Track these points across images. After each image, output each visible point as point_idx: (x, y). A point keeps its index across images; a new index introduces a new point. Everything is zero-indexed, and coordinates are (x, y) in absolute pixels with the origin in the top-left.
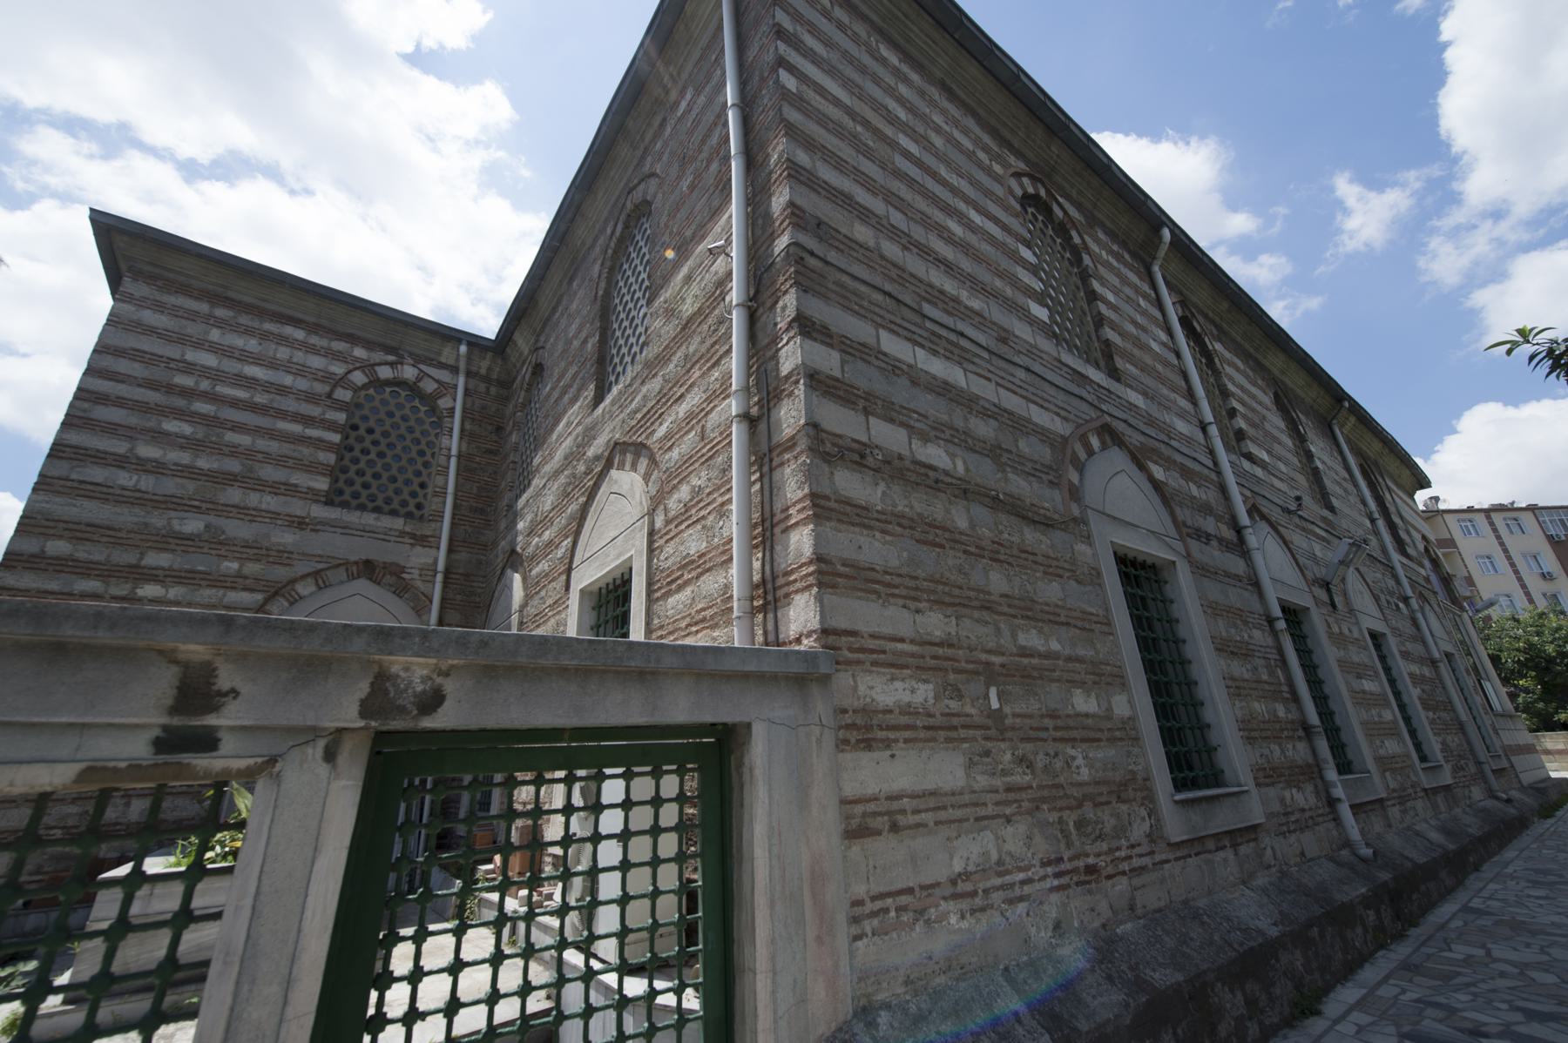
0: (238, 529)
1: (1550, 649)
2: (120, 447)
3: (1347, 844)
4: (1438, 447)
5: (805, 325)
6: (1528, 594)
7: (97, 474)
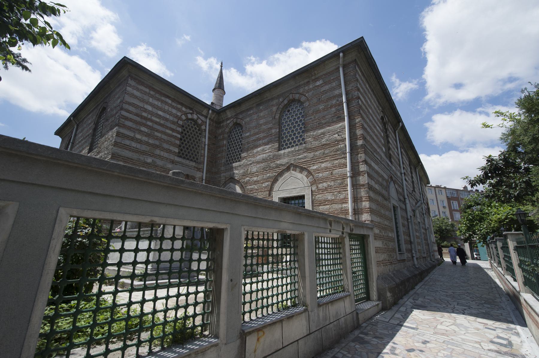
0: (159, 162)
1: (444, 227)
2: (132, 134)
3: (414, 265)
4: (324, 40)
5: (365, 162)
6: (439, 211)
7: (127, 142)
